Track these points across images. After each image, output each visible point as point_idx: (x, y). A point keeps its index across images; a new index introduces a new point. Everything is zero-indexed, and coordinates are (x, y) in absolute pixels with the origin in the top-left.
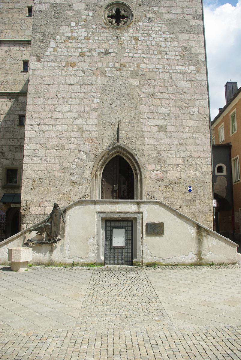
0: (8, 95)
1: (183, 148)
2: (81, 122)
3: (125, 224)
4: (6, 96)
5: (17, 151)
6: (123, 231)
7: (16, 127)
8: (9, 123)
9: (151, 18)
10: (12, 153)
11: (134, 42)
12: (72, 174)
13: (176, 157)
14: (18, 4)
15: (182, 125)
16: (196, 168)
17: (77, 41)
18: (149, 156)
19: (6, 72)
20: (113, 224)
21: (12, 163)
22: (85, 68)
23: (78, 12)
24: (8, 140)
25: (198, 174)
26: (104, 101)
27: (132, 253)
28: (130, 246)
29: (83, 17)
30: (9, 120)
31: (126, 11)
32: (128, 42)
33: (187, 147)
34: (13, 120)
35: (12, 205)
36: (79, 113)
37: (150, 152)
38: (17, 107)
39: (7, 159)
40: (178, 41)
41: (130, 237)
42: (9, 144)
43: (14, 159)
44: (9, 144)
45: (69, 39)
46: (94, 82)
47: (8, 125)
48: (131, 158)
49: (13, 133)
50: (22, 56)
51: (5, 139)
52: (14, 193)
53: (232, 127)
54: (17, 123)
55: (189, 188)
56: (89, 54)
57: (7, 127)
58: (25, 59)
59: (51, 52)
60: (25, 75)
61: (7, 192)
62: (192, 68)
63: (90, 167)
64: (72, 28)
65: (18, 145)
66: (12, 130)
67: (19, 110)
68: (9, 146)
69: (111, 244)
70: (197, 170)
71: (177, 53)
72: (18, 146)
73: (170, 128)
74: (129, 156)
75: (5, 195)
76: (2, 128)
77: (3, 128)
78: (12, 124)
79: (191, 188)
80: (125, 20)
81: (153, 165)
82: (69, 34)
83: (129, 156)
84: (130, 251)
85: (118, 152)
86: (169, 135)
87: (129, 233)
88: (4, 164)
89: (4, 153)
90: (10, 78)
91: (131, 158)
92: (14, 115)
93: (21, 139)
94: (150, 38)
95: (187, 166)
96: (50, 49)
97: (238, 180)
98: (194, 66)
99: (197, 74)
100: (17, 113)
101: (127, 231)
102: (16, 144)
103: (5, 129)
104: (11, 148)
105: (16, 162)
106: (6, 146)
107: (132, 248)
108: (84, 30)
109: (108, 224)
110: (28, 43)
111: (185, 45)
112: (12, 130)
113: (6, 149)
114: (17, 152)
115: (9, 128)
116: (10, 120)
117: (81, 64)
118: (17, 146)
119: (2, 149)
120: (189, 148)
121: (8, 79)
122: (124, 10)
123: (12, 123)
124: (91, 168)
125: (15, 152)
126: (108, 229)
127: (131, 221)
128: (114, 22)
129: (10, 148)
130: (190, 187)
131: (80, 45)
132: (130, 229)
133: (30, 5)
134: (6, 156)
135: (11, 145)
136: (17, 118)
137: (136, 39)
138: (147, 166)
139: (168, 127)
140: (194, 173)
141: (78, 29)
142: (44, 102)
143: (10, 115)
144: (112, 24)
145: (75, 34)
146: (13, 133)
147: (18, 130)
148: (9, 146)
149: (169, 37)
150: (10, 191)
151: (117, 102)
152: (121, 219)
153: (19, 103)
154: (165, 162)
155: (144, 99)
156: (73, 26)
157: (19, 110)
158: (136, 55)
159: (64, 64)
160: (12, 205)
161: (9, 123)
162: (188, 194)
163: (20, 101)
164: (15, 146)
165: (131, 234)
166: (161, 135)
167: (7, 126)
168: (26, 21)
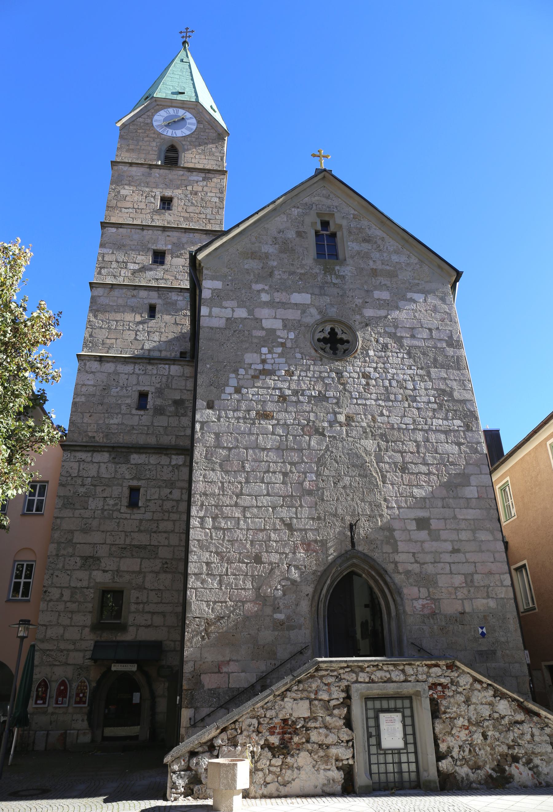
0: (111, 450)
1: (460, 557)
2: (284, 513)
3: (399, 703)
4: (108, 451)
5: (124, 555)
6: (398, 717)
7: (124, 509)
8: (111, 502)
9: (385, 343)
10: (115, 559)
11: (363, 381)
12: (276, 609)
13: (451, 573)
14: (134, 300)
15: (455, 517)
16: (488, 592)
17: (273, 377)
18: (408, 573)
19: (109, 411)
20: (378, 704)
21: (114, 578)
22: (288, 422)
23: (272, 332)
24: (108, 534)
25: (492, 604)
26: (324, 478)
27: (417, 762)
28: (411, 748)
29: (280, 340)
30: (111, 497)
31: (345, 333)
32: (354, 381)
33: (468, 555)
34: (117, 496)
35: (114, 666)
36: (284, 497)
37: (410, 567)
38: (126, 472)
39: (104, 571)
40: (431, 379)
41: (409, 730)
42: (108, 541)
43: (117, 571)
44: (108, 541)
45: (260, 374)
46: (305, 445)
47: (108, 505)
48: (377, 577)
49: (118, 521)
50: (138, 384)
51: (103, 532)
52: (114, 639)
53: (505, 509)
54: (125, 502)
55: (480, 631)
56: (294, 399)
57: (106, 510)
58: (143, 389)
59: (230, 394)
60: (142, 416)
61: (101, 637)
62: (458, 422)
63: (307, 595)
64: (263, 357)
65: (126, 543)
66: (115, 514)
67: (131, 479)
68: (109, 546)
69: (379, 744)
70: (488, 597)
71: (432, 399)
72: (125, 546)
73: (434, 524)
74: (373, 573)
75: (98, 645)
76: (98, 510)
77: (99, 512)
78: (116, 504)
79: (484, 630)
80: (346, 346)
81: (416, 589)
82: (260, 367)
83: (373, 573)
84: (412, 758)
85: (354, 565)
86: (435, 536)
87: (408, 721)
88: (98, 581)
89: (98, 559)
90: (115, 421)
91: (377, 577)
92: (120, 488)
93: (132, 534)
94: (388, 375)
95: (472, 590)
96: (229, 390)
97: (531, 605)
98: (460, 419)
99: (466, 433)
100: (126, 484)
101: (404, 717)
102: (123, 543)
103: (103, 513)
104: (113, 549)
105: (121, 576)
106: (104, 546)
107: (416, 753)
108: (283, 360)
109: (370, 704)
110: (148, 362)
111: (443, 387)
112: (115, 514)
113: (102, 551)
114: (123, 557)
115: (111, 512)
116: (113, 496)
117: (282, 415)
118: (123, 546)
119: (95, 551)
120: (471, 557)
121: (112, 422)
122: (342, 331)
123: (117, 501)
124: (310, 596)
125: (121, 558)
126: (371, 714)
127: (410, 698)
128: (328, 349)
129: (110, 550)
130: (482, 628)
131: (280, 385)
132: (408, 712)
133: (153, 302)
134: (103, 565)
135: (113, 543)
136: (126, 492)
137: (366, 376)
138: (405, 591)
139: (432, 521)
140: (485, 601)
141: (273, 358)
142: (223, 478)
143: (114, 488)
144: (325, 352)
145: (267, 367)
146: (118, 521)
147: (128, 516)
148: (109, 546)
149: (417, 374)
150: (106, 636)
151: (347, 480)
152: (392, 694)
153: (130, 466)
154: (435, 584)
155: (388, 475)
156: (265, 354)
157: (131, 479)
158: (368, 402)
159: (253, 414)
160: (114, 666)
161: (111, 502)
162: (480, 640)
163: (132, 462)
164: (120, 546)
165: (410, 723)
166: (423, 535)
167: (106, 507)
168: (146, 325)
